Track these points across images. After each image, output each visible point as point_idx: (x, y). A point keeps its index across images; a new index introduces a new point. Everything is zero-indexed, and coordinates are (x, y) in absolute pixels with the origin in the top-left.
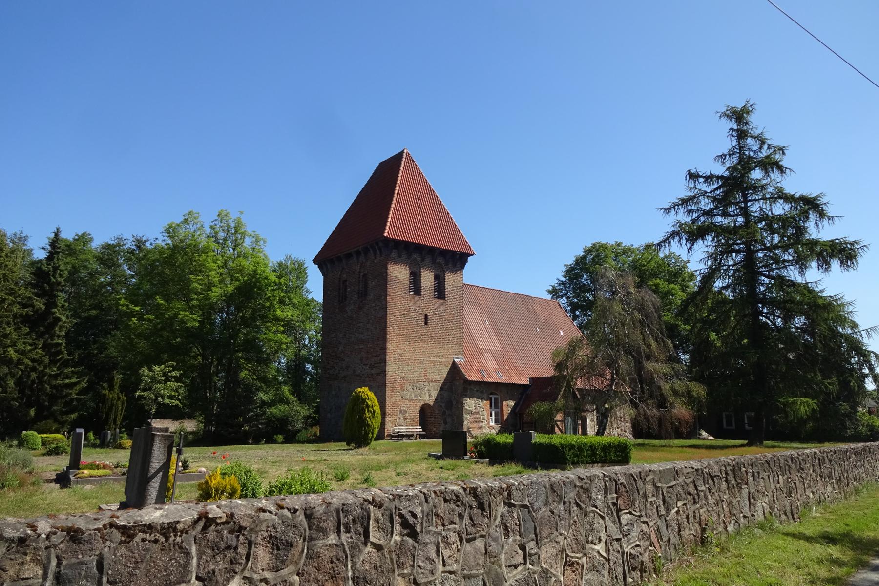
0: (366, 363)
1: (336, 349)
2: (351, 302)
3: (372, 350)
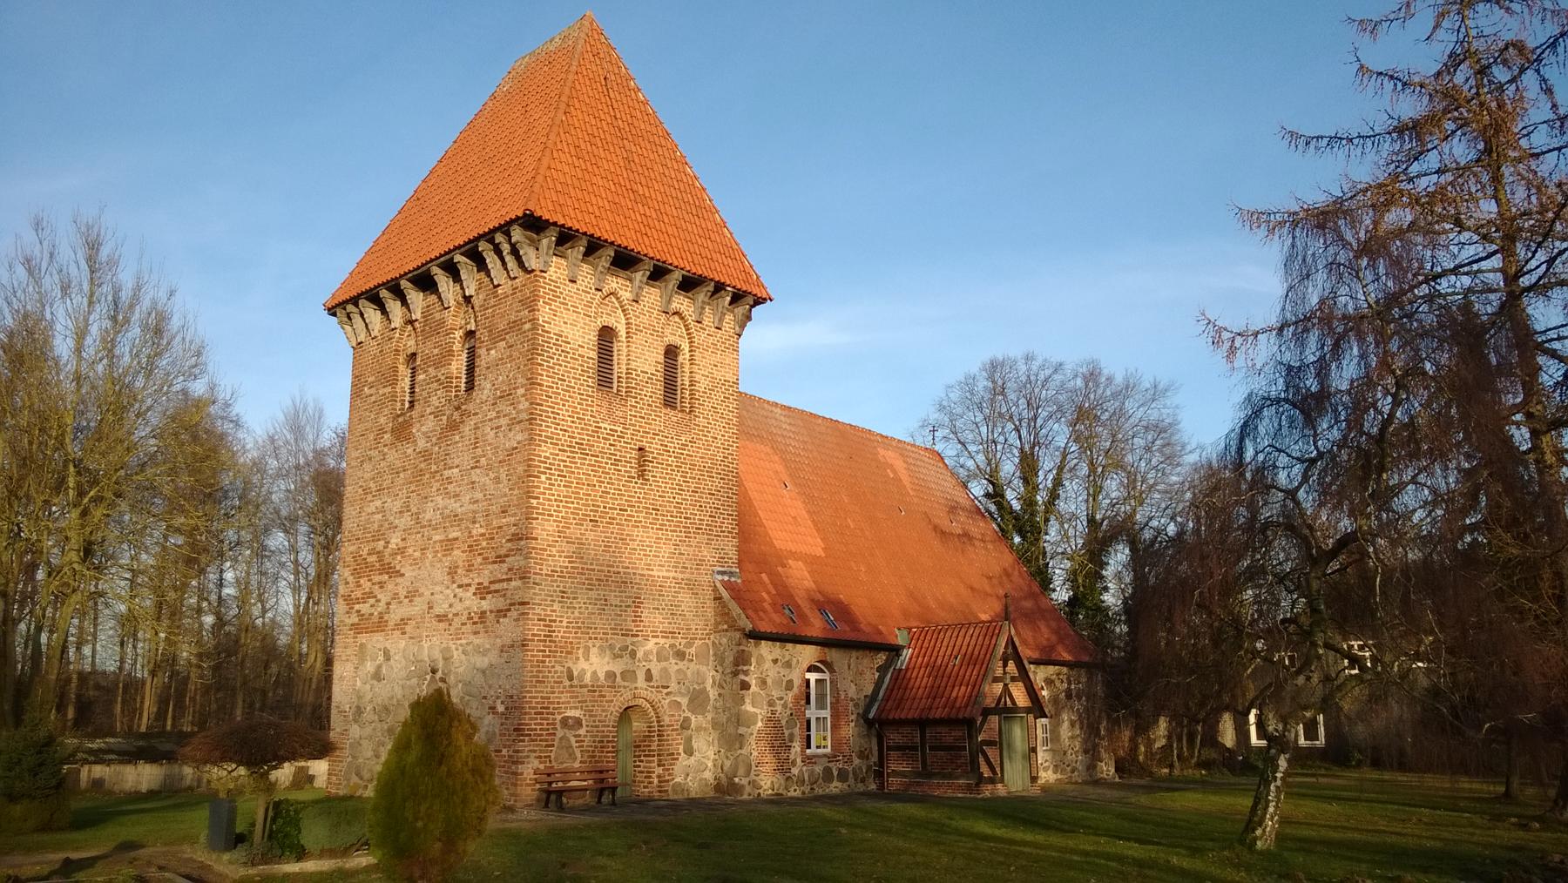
0: (466, 581)
1: (382, 543)
2: (428, 411)
3: (484, 544)
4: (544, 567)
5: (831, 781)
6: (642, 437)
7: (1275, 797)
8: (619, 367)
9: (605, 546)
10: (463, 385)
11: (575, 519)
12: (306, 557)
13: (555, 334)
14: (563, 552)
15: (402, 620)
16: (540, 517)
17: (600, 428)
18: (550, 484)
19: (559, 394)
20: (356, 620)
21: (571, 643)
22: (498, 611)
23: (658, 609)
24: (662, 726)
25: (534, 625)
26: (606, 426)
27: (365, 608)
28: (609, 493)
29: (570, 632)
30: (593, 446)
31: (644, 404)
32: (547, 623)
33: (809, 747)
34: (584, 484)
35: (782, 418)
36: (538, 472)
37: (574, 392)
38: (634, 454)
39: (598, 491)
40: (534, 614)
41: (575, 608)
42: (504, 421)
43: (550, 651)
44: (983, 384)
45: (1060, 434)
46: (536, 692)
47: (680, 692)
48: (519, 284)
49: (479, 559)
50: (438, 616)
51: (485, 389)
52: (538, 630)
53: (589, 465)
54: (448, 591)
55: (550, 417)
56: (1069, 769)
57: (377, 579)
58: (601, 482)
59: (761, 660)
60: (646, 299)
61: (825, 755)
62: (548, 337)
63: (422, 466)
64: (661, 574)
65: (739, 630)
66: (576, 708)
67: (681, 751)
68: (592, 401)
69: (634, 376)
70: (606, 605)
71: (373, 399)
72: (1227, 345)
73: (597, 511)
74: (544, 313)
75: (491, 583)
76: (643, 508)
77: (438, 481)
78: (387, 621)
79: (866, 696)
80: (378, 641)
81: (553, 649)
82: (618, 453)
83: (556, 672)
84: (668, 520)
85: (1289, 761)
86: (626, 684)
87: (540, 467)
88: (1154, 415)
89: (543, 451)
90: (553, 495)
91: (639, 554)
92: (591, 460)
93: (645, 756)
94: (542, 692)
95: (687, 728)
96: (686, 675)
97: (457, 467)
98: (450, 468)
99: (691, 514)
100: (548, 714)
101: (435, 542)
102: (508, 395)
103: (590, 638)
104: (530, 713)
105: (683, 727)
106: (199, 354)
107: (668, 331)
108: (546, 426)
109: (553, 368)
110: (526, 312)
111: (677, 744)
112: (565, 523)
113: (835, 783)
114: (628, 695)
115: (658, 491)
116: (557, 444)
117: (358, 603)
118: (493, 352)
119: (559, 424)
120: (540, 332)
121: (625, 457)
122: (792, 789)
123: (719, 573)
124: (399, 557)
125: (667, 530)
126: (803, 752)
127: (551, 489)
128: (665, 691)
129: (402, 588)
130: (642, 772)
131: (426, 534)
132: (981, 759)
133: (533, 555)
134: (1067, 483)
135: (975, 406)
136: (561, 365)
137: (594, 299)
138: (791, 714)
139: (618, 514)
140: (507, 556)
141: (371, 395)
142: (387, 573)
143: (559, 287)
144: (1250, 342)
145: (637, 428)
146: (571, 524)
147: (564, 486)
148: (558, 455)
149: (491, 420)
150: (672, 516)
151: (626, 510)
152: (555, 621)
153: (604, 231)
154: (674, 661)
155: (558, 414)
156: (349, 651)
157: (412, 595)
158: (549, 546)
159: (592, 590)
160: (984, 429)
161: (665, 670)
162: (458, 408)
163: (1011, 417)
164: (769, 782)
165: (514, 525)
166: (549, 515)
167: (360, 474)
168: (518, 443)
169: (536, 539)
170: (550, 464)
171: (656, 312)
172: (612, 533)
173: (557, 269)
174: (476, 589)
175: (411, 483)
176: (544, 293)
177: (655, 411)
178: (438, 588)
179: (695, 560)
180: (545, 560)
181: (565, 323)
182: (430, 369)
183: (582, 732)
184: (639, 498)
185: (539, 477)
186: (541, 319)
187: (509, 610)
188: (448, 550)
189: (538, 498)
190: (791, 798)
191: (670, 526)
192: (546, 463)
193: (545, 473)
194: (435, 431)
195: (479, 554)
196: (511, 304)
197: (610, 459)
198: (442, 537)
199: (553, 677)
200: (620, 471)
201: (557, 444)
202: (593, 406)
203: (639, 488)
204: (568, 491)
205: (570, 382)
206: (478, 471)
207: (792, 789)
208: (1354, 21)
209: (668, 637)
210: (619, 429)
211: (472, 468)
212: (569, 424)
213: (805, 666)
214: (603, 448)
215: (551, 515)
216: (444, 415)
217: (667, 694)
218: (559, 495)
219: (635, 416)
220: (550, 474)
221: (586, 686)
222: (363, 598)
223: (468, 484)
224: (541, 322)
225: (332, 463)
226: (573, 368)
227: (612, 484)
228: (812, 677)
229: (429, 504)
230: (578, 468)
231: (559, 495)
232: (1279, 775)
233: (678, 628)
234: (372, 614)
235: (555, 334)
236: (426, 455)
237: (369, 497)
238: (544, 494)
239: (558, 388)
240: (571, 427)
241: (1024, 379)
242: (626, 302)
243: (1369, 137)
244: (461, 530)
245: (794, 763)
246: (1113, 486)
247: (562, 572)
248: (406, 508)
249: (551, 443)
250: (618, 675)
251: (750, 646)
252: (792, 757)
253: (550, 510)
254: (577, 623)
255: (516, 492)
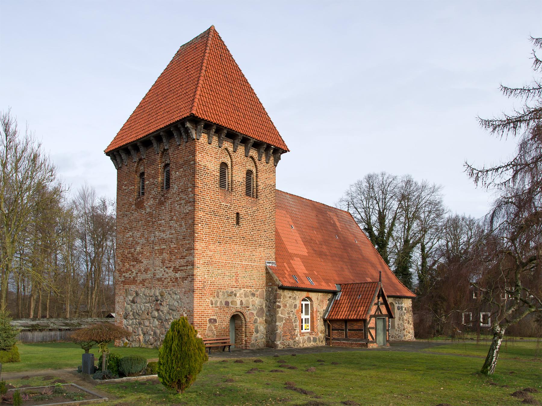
0: (169, 265)
2: (150, 196)
4: (201, 261)
5: (310, 342)
6: (238, 208)
7: (496, 355)
8: (228, 179)
9: (224, 252)
10: (165, 186)
11: (212, 242)
12: (90, 249)
13: (203, 166)
14: (208, 255)
15: (143, 280)
16: (199, 241)
17: (221, 204)
18: (202, 228)
19: (205, 191)
20: (123, 279)
21: (212, 290)
22: (183, 278)
23: (245, 277)
24: (247, 322)
25: (198, 284)
26: (224, 204)
27: (127, 275)
28: (225, 231)
29: (211, 286)
30: (219, 212)
31: (238, 195)
32: (203, 283)
33: (302, 329)
34: (215, 228)
35: (290, 199)
36: (198, 223)
37: (211, 190)
38: (235, 215)
39: (221, 230)
40: (197, 279)
41: (213, 277)
42: (183, 202)
43: (204, 294)
44: (365, 184)
45: (395, 205)
46: (199, 309)
47: (253, 309)
48: (188, 145)
49: (174, 257)
50: (158, 279)
51: (175, 188)
52: (199, 285)
53: (217, 220)
54: (162, 269)
55: (202, 200)
56: (397, 336)
57: (132, 263)
58: (222, 227)
59: (285, 297)
60: (239, 151)
61: (308, 333)
62: (201, 167)
63: (149, 219)
64: (245, 263)
65: (276, 286)
66: (214, 315)
67: (254, 331)
68: (218, 194)
69: (234, 183)
70: (225, 276)
71: (127, 191)
72: (475, 176)
73: (221, 238)
74: (199, 157)
75: (179, 267)
76: (239, 237)
77: (156, 225)
78: (136, 280)
79: (324, 310)
80: (133, 288)
81: (205, 293)
82: (229, 215)
83: (206, 302)
84: (248, 242)
85: (502, 342)
86: (233, 306)
87: (198, 221)
88: (432, 198)
89: (200, 214)
90: (204, 232)
91: (237, 256)
92: (218, 218)
93: (240, 333)
94: (202, 309)
95: (256, 323)
96: (255, 302)
97: (163, 220)
98: (161, 220)
99: (257, 239)
100: (203, 317)
101: (156, 250)
102: (184, 191)
103: (219, 289)
104: (197, 317)
105: (254, 322)
106: (52, 171)
107: (247, 164)
108: (201, 204)
109: (202, 180)
110: (191, 156)
111: (252, 329)
112: (209, 243)
113: (312, 343)
114: (234, 310)
115: (244, 230)
116: (205, 211)
117: (124, 273)
118: (177, 173)
119: (205, 203)
120: (197, 165)
121: (231, 216)
122: (296, 345)
123: (268, 263)
124: (140, 255)
125: (248, 246)
126: (300, 331)
127: (203, 230)
128: (248, 309)
129: (142, 267)
130: (239, 339)
131: (152, 246)
132: (369, 334)
133: (197, 256)
134: (397, 225)
135: (362, 193)
136: (206, 179)
137: (218, 151)
138: (296, 317)
139: (229, 240)
140: (186, 256)
141: (126, 189)
142: (136, 261)
143: (204, 146)
144: (484, 175)
145: (236, 205)
146: (211, 244)
147: (208, 228)
148: (205, 216)
149: (177, 201)
150: (250, 240)
151: (232, 238)
152: (205, 282)
153: (223, 122)
154: (251, 297)
155: (205, 199)
156: (121, 292)
157: (146, 270)
158: (202, 252)
159: (219, 270)
160: (365, 203)
161: (248, 301)
162: (163, 196)
163: (376, 198)
164: (287, 343)
165: (189, 244)
166: (202, 240)
167: (122, 221)
168: (189, 211)
169: (198, 250)
170: (202, 219)
171: (243, 156)
172: (227, 247)
173: (203, 138)
174: (173, 269)
175: (144, 226)
176: (199, 149)
177: (243, 198)
178: (157, 268)
179: (259, 258)
180: (201, 258)
181: (207, 161)
182: (151, 179)
183: (217, 324)
184: (237, 233)
185: (198, 225)
186: (198, 160)
187: (188, 278)
188: (161, 253)
189: (198, 233)
190: (296, 349)
191: (249, 244)
192: (201, 219)
193: (200, 223)
194: (154, 205)
195: (174, 255)
196: (185, 153)
197: (226, 217)
198: (159, 248)
199: (205, 304)
200: (229, 222)
201: (205, 211)
202: (218, 196)
203: (237, 229)
204: (209, 231)
205: (209, 186)
206: (172, 221)
207: (296, 345)
208: (534, 39)
209: (248, 288)
210: (229, 205)
211: (170, 220)
212: (209, 203)
213: (301, 299)
214: (223, 213)
215: (203, 240)
216: (158, 198)
217: (248, 310)
218: (206, 232)
219: (235, 200)
220: (202, 223)
221: (218, 307)
222: (126, 271)
223: (168, 227)
224: (197, 161)
225: (99, 212)
226: (211, 180)
227: (226, 227)
228: (304, 303)
229: (152, 234)
230: (213, 221)
231: (206, 232)
232: (498, 347)
233: (252, 285)
234: (130, 277)
235: (203, 166)
236: (150, 214)
237: (127, 231)
238: (200, 231)
239: (205, 188)
240: (210, 204)
241: (381, 183)
242: (231, 152)
243: (538, 89)
244: (166, 245)
245: (297, 336)
246: (415, 226)
247: (208, 263)
248: (143, 235)
249: (203, 211)
250: (230, 303)
251: (280, 292)
252: (296, 333)
253: (203, 238)
254: (214, 283)
255: (189, 231)
